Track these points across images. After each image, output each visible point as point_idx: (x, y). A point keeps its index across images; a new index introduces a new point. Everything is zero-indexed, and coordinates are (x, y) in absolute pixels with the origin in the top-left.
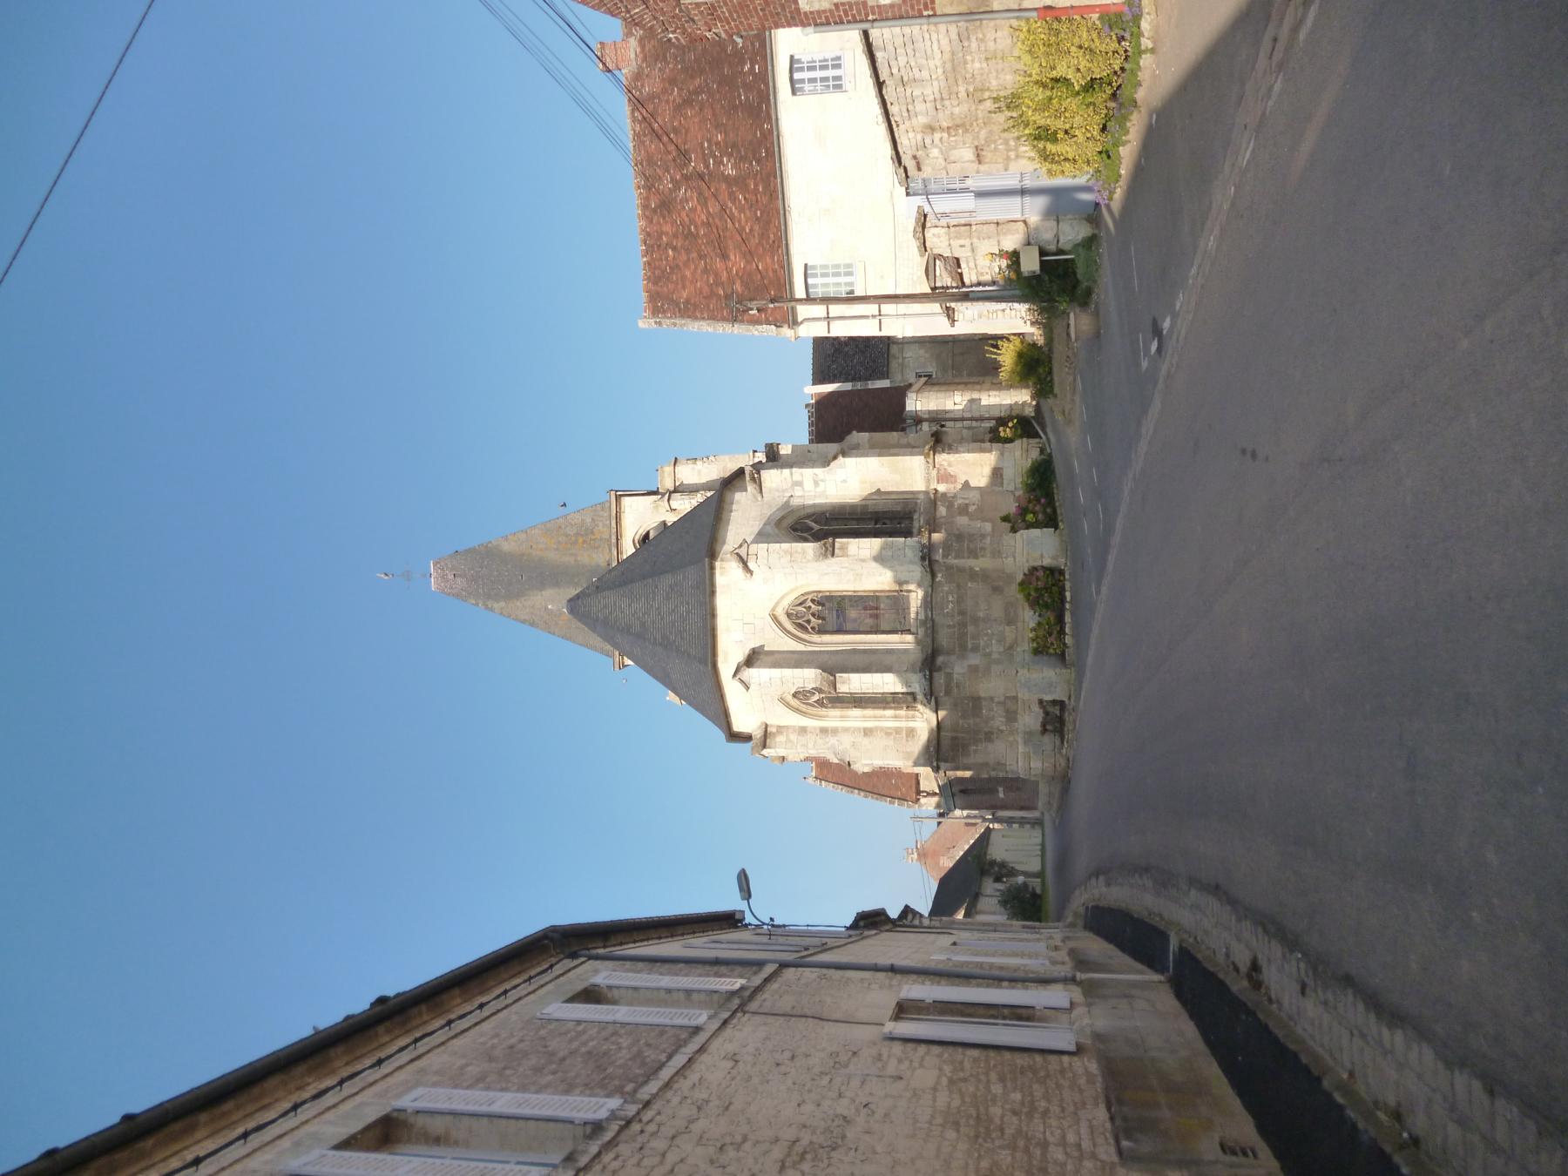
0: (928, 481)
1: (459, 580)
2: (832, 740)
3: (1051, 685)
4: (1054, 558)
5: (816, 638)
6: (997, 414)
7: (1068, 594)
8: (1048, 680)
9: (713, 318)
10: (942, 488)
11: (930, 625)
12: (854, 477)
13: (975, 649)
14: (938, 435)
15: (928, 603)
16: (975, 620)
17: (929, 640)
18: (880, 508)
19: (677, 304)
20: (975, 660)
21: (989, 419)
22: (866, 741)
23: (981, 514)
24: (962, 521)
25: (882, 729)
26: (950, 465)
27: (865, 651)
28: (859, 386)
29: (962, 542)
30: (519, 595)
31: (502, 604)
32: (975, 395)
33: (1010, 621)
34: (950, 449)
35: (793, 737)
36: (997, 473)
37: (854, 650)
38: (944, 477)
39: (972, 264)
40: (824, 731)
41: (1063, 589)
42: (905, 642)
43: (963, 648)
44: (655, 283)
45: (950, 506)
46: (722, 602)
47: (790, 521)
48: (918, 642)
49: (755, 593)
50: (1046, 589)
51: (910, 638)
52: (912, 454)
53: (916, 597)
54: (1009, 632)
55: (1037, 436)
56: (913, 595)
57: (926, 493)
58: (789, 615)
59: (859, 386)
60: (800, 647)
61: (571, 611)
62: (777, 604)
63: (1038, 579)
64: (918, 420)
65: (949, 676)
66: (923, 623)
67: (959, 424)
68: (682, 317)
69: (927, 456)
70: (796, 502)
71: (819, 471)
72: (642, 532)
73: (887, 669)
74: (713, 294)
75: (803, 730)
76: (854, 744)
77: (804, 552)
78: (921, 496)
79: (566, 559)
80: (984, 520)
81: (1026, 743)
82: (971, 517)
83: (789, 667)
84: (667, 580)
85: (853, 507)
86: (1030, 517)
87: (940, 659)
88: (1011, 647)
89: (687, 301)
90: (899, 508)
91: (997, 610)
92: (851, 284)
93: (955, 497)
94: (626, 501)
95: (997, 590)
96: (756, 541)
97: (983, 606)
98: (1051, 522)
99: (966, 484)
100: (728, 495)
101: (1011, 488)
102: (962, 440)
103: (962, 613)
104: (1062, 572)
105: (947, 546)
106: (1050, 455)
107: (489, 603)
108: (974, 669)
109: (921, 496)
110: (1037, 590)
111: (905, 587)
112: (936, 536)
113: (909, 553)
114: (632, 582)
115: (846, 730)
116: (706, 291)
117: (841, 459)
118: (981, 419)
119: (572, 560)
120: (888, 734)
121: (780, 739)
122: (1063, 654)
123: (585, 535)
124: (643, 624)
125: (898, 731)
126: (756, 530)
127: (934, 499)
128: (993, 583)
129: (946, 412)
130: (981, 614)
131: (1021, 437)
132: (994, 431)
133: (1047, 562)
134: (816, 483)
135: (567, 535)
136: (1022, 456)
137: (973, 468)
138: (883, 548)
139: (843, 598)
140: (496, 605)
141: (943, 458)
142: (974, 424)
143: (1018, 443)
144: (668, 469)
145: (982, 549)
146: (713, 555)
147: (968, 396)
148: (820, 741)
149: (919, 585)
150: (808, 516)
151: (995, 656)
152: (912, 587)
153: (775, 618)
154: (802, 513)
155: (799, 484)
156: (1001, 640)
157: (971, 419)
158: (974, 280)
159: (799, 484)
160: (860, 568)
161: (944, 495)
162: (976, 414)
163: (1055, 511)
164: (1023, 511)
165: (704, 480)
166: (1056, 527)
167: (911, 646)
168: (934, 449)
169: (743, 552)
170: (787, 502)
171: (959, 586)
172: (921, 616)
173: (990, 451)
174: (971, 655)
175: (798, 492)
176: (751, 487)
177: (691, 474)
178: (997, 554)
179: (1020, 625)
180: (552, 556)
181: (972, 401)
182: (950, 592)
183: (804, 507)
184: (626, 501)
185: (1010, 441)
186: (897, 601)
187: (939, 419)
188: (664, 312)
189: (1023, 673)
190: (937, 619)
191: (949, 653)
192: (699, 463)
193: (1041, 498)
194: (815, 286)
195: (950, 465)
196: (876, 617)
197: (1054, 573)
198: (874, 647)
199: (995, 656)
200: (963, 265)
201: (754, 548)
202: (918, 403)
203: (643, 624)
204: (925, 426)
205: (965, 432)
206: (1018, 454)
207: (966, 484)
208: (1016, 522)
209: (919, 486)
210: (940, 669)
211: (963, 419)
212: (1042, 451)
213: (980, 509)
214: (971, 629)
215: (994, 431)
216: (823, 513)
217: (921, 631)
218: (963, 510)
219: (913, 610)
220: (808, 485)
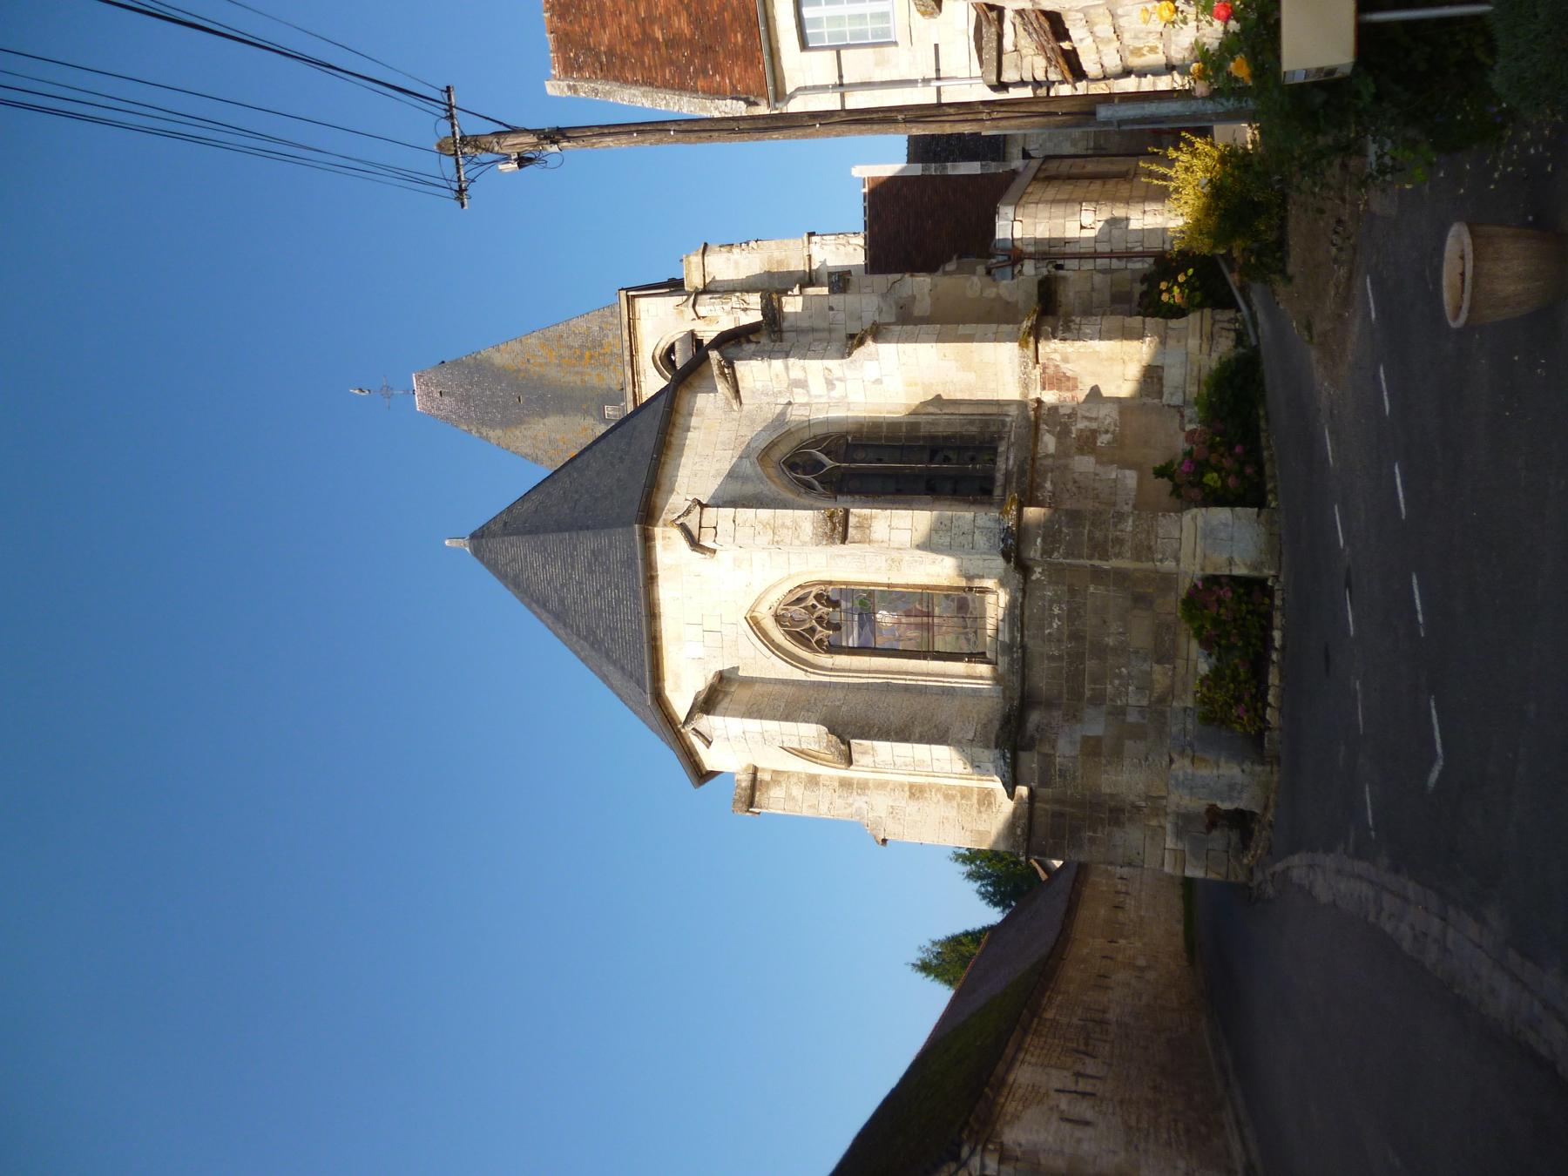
0: (1026, 386)
1: (446, 400)
2: (859, 802)
3: (1232, 787)
4: (1254, 567)
5: (825, 659)
6: (1155, 245)
7: (1277, 634)
8: (1227, 779)
9: (649, 82)
10: (1050, 397)
11: (1016, 655)
12: (891, 380)
13: (1098, 700)
14: (1049, 302)
15: (1016, 615)
16: (1100, 651)
17: (1016, 680)
18: (940, 430)
19: (597, 55)
20: (1095, 725)
21: (1142, 255)
22: (912, 807)
23: (1117, 455)
24: (1084, 464)
25: (939, 789)
26: (1066, 360)
27: (906, 688)
28: (933, 169)
29: (1083, 523)
30: (519, 422)
31: (499, 432)
32: (1120, 212)
33: (1164, 655)
34: (1068, 331)
35: (797, 791)
36: (1152, 376)
37: (888, 687)
38: (1055, 380)
39: (1104, 28)
40: (846, 784)
41: (1267, 629)
42: (975, 676)
43: (1076, 694)
44: (562, 17)
45: (1063, 434)
46: (666, 593)
47: (784, 450)
48: (997, 679)
49: (722, 585)
50: (1231, 615)
51: (984, 669)
52: (997, 339)
53: (996, 603)
54: (1160, 676)
55: (1232, 304)
56: (990, 598)
57: (1022, 405)
58: (778, 619)
59: (933, 169)
60: (798, 675)
61: (476, 552)
62: (758, 602)
63: (1220, 602)
64: (1015, 255)
65: (1047, 759)
66: (1008, 648)
67: (1088, 265)
68: (605, 78)
69: (1024, 344)
70: (796, 415)
71: (834, 365)
72: (664, 345)
73: (936, 736)
74: (647, 38)
75: (813, 781)
76: (892, 811)
77: (797, 527)
78: (1013, 411)
79: (570, 378)
80: (1125, 465)
81: (1179, 834)
82: (1103, 458)
83: (774, 718)
84: (588, 542)
85: (894, 425)
86: (1211, 478)
87: (1035, 717)
88: (1161, 700)
89: (611, 52)
90: (974, 430)
91: (1140, 634)
92: (884, 16)
93: (1072, 415)
94: (642, 304)
95: (1141, 600)
96: (719, 502)
97: (1115, 627)
98: (1249, 494)
99: (1095, 392)
100: (685, 396)
101: (1177, 400)
102: (1087, 312)
103: (1076, 636)
104: (1261, 582)
105: (1049, 531)
106: (1256, 350)
107: (484, 431)
108: (1092, 748)
109: (1013, 411)
110: (1217, 622)
111: (977, 583)
112: (1032, 513)
113: (980, 540)
114: (546, 531)
115: (881, 785)
116: (636, 30)
117: (870, 346)
118: (1128, 255)
119: (578, 379)
120: (948, 797)
121: (776, 793)
122: (1260, 735)
123: (593, 349)
124: (562, 600)
125: (965, 793)
126: (727, 467)
127: (1036, 417)
128: (1140, 592)
129: (1066, 242)
130: (1110, 641)
131: (1201, 306)
132: (1142, 289)
133: (1240, 571)
134: (830, 384)
135: (570, 347)
136: (1197, 348)
137: (1107, 366)
138: (935, 529)
139: (871, 593)
140: (491, 434)
141: (1052, 349)
142: (1115, 264)
143: (1193, 319)
144: (696, 259)
145: (1119, 541)
146: (648, 515)
147: (1105, 213)
148: (839, 802)
149: (1002, 584)
150: (817, 442)
151: (1133, 717)
152: (989, 583)
153: (755, 624)
154: (806, 435)
155: (802, 384)
156: (1145, 686)
157: (1111, 255)
158: (1113, 63)
159: (802, 384)
160: (897, 548)
161: (1054, 409)
162: (1120, 247)
163: (1260, 466)
164: (1199, 466)
165: (742, 276)
166: (1260, 503)
167: (985, 685)
168: (1037, 333)
169: (692, 522)
170: (783, 414)
171: (1072, 591)
172: (1004, 637)
173: (1140, 336)
174: (1089, 712)
175: (799, 397)
176: (722, 387)
177: (727, 266)
178: (1144, 550)
179: (1180, 663)
180: (553, 373)
181: (1112, 222)
182: (1056, 600)
183: (810, 424)
184: (642, 304)
185: (1176, 312)
186: (964, 602)
187: (1052, 253)
188: (580, 69)
189: (1182, 767)
190: (1030, 643)
191: (1050, 705)
192: (736, 250)
193: (1232, 437)
194: (817, 22)
195: (1066, 360)
196: (929, 628)
197: (1251, 587)
198: (920, 681)
199: (1133, 717)
200: (1077, 31)
201: (710, 513)
202: (1019, 225)
203: (562, 600)
204: (1029, 267)
205: (1098, 278)
206: (1193, 343)
207: (1095, 392)
208: (1188, 483)
209: (1011, 392)
210: (1030, 746)
211: (1095, 255)
212: (1240, 339)
213: (1118, 441)
214: (1090, 664)
215: (1142, 289)
216: (842, 436)
217: (1003, 662)
218: (1087, 442)
219: (990, 624)
220: (817, 386)
